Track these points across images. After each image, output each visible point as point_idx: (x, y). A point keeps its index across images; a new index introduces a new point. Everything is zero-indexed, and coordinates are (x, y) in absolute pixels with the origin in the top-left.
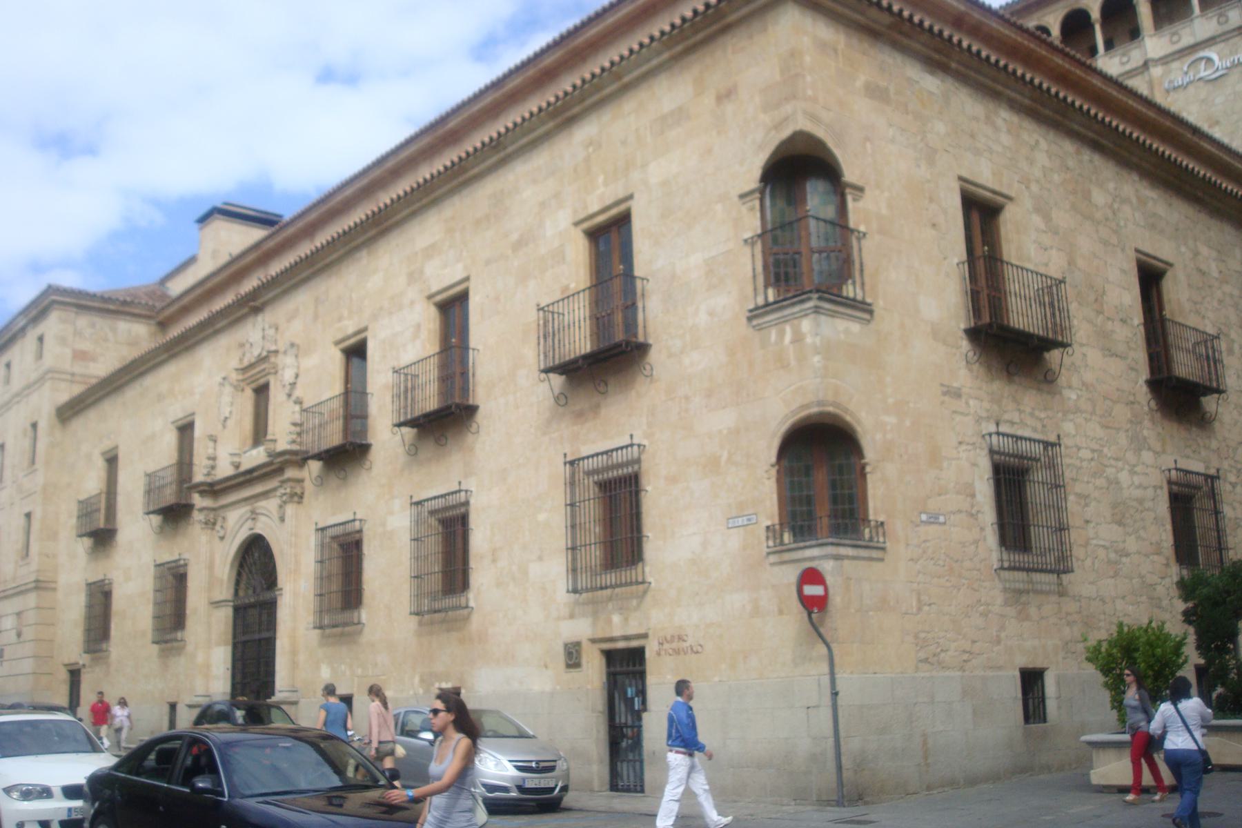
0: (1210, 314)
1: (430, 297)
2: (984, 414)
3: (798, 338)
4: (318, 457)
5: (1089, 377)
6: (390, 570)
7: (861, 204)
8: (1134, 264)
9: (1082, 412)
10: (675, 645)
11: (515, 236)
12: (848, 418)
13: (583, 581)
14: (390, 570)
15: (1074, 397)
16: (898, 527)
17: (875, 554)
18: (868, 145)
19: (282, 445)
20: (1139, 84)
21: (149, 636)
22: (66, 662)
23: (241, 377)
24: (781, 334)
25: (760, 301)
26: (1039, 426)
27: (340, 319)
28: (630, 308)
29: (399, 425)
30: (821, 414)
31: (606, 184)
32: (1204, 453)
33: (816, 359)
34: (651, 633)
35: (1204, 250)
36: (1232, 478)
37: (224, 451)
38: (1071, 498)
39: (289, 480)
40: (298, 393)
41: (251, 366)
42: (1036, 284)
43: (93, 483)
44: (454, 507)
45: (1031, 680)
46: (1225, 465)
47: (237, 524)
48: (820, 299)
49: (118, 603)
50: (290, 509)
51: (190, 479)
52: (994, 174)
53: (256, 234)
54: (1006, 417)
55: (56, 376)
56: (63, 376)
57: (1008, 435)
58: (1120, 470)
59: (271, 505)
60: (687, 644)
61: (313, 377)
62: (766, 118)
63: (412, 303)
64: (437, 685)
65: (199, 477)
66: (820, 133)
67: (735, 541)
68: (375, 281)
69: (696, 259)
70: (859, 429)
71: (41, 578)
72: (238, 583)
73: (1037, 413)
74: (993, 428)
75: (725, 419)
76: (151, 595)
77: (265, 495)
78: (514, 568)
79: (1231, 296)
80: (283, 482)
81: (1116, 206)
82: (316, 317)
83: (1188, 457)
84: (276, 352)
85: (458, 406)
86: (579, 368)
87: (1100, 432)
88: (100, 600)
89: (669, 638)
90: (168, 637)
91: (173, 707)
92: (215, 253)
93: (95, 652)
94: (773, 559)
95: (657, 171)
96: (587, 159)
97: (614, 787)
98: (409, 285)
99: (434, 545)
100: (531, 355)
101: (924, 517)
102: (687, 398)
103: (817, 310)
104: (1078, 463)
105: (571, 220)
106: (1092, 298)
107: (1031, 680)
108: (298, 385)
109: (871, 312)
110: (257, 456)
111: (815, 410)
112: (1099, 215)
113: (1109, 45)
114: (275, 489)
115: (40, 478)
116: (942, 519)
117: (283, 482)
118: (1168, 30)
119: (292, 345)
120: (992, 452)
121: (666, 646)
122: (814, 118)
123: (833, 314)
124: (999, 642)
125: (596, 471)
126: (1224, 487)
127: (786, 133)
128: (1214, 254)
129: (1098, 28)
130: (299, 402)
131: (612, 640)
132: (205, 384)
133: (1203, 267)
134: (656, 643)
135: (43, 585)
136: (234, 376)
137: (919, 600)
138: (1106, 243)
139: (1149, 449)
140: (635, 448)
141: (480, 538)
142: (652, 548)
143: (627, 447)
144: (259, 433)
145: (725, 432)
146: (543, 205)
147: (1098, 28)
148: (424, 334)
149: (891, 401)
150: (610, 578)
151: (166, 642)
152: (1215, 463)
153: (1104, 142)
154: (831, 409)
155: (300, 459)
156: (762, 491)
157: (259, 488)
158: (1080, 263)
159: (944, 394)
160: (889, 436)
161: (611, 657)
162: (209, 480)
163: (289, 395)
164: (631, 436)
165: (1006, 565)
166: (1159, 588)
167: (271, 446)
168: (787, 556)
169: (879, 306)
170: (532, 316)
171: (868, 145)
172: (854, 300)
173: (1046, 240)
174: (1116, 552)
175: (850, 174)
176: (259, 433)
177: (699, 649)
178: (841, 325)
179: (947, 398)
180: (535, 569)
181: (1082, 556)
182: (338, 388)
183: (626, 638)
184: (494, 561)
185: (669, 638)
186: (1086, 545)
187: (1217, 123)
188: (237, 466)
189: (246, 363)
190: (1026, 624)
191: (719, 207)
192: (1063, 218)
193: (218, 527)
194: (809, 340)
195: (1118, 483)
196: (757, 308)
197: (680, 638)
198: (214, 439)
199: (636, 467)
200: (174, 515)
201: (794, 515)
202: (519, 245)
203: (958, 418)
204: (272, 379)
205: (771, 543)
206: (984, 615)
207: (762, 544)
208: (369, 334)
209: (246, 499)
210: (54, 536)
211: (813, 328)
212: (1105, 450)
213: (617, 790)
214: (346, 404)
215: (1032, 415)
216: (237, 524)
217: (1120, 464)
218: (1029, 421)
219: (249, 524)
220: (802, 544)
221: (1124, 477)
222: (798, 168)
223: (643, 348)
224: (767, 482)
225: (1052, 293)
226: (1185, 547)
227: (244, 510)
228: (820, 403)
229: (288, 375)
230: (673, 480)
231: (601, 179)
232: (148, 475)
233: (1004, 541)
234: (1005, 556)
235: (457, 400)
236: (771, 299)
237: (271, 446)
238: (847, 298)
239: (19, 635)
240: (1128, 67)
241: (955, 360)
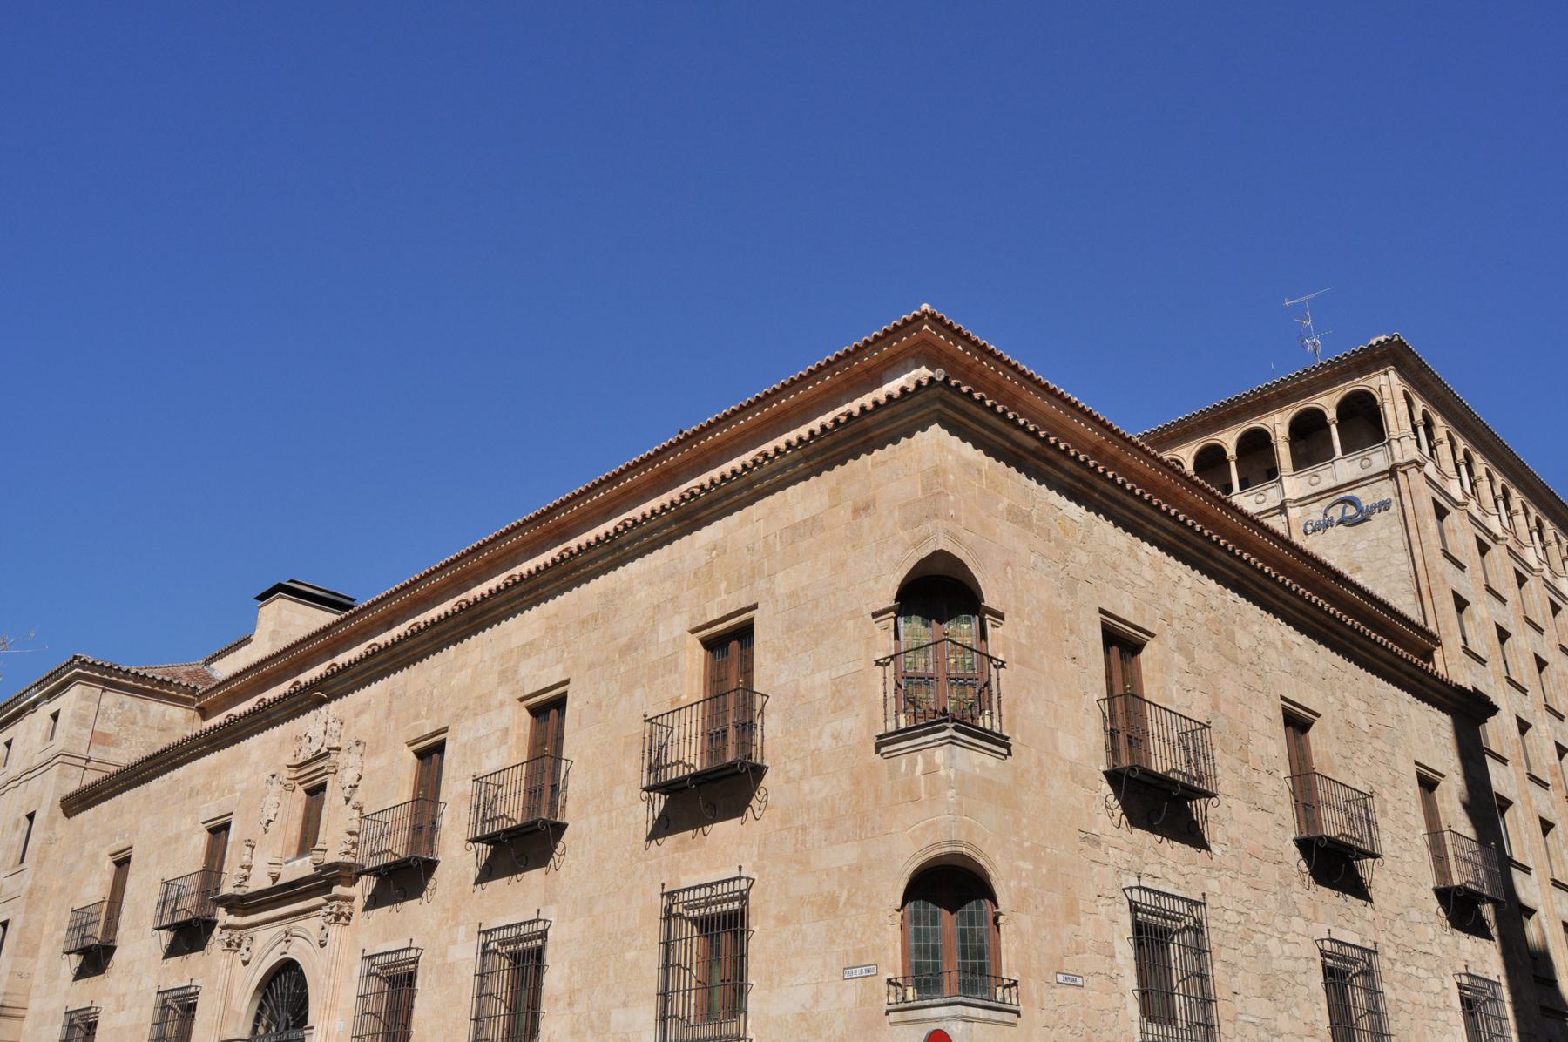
0: (1360, 771)
1: (522, 699)
2: (1124, 866)
3: (930, 770)
4: (375, 872)
5: (1233, 831)
7: (999, 631)
8: (1280, 712)
9: (1228, 869)
11: (624, 640)
12: (981, 861)
16: (1031, 987)
17: (1007, 1017)
18: (1009, 569)
19: (331, 857)
20: (1276, 523)
23: (293, 775)
24: (913, 764)
26: (1182, 881)
27: (417, 717)
28: (747, 727)
29: (474, 841)
30: (953, 855)
31: (728, 592)
32: (1358, 924)
33: (951, 793)
35: (1353, 703)
36: (1390, 953)
37: (262, 861)
38: (1217, 965)
39: (336, 898)
40: (357, 797)
41: (307, 763)
42: (1179, 726)
43: (95, 889)
46: (1382, 939)
47: (267, 944)
48: (956, 729)
50: (334, 931)
51: (218, 889)
53: (325, 618)
54: (1148, 870)
55: (68, 759)
56: (77, 761)
57: (1149, 890)
59: (312, 925)
61: (377, 781)
62: (904, 535)
63: (502, 704)
65: (227, 889)
66: (961, 554)
69: (823, 677)
70: (992, 874)
72: (258, 1018)
73: (1179, 867)
74: (1134, 882)
79: (1383, 752)
80: (330, 900)
81: (1260, 649)
83: (1342, 927)
84: (339, 749)
85: (544, 822)
87: (1247, 894)
92: (274, 634)
95: (784, 583)
96: (710, 564)
98: (500, 684)
99: (501, 983)
100: (634, 773)
101: (1060, 978)
103: (952, 740)
104: (1223, 926)
105: (688, 627)
106: (1236, 746)
109: (1008, 747)
110: (303, 867)
112: (1242, 658)
113: (1244, 485)
114: (319, 907)
115: (27, 880)
116: (1079, 981)
118: (1307, 473)
119: (358, 743)
120: (1134, 908)
122: (955, 538)
123: (969, 746)
126: (1382, 963)
127: (926, 551)
128: (1364, 706)
129: (1233, 464)
132: (250, 779)
136: (285, 774)
138: (1250, 688)
139: (1300, 915)
142: (753, 1000)
144: (308, 840)
146: (657, 608)
147: (1233, 464)
148: (512, 740)
149: (1027, 844)
154: (964, 850)
155: (343, 873)
156: (885, 939)
158: (1223, 707)
159: (1083, 840)
160: (1024, 884)
162: (239, 892)
163: (348, 800)
167: (319, 856)
168: (910, 1015)
170: (638, 727)
171: (1009, 569)
172: (991, 732)
173: (1189, 680)
174: (1267, 1030)
175: (990, 600)
176: (308, 840)
178: (977, 757)
179: (1085, 845)
180: (617, 1017)
181: (1230, 1034)
182: (407, 794)
186: (1235, 1021)
187: (1359, 569)
188: (275, 880)
189: (301, 759)
191: (850, 624)
192: (1206, 659)
193: (243, 950)
194: (942, 772)
196: (887, 735)
200: (188, 936)
201: (918, 968)
202: (626, 650)
203: (1097, 867)
204: (329, 779)
207: (883, 997)
210: (32, 951)
211: (950, 759)
212: (1253, 913)
214: (416, 815)
217: (1269, 930)
218: (1172, 876)
219: (282, 947)
220: (927, 1002)
221: (1273, 944)
222: (938, 591)
223: (759, 771)
224: (890, 928)
225: (1194, 736)
227: (277, 930)
228: (951, 843)
230: (784, 920)
231: (723, 586)
232: (166, 883)
233: (1147, 1013)
235: (544, 817)
237: (319, 856)
238: (984, 730)
240: (1264, 507)
241: (1100, 807)
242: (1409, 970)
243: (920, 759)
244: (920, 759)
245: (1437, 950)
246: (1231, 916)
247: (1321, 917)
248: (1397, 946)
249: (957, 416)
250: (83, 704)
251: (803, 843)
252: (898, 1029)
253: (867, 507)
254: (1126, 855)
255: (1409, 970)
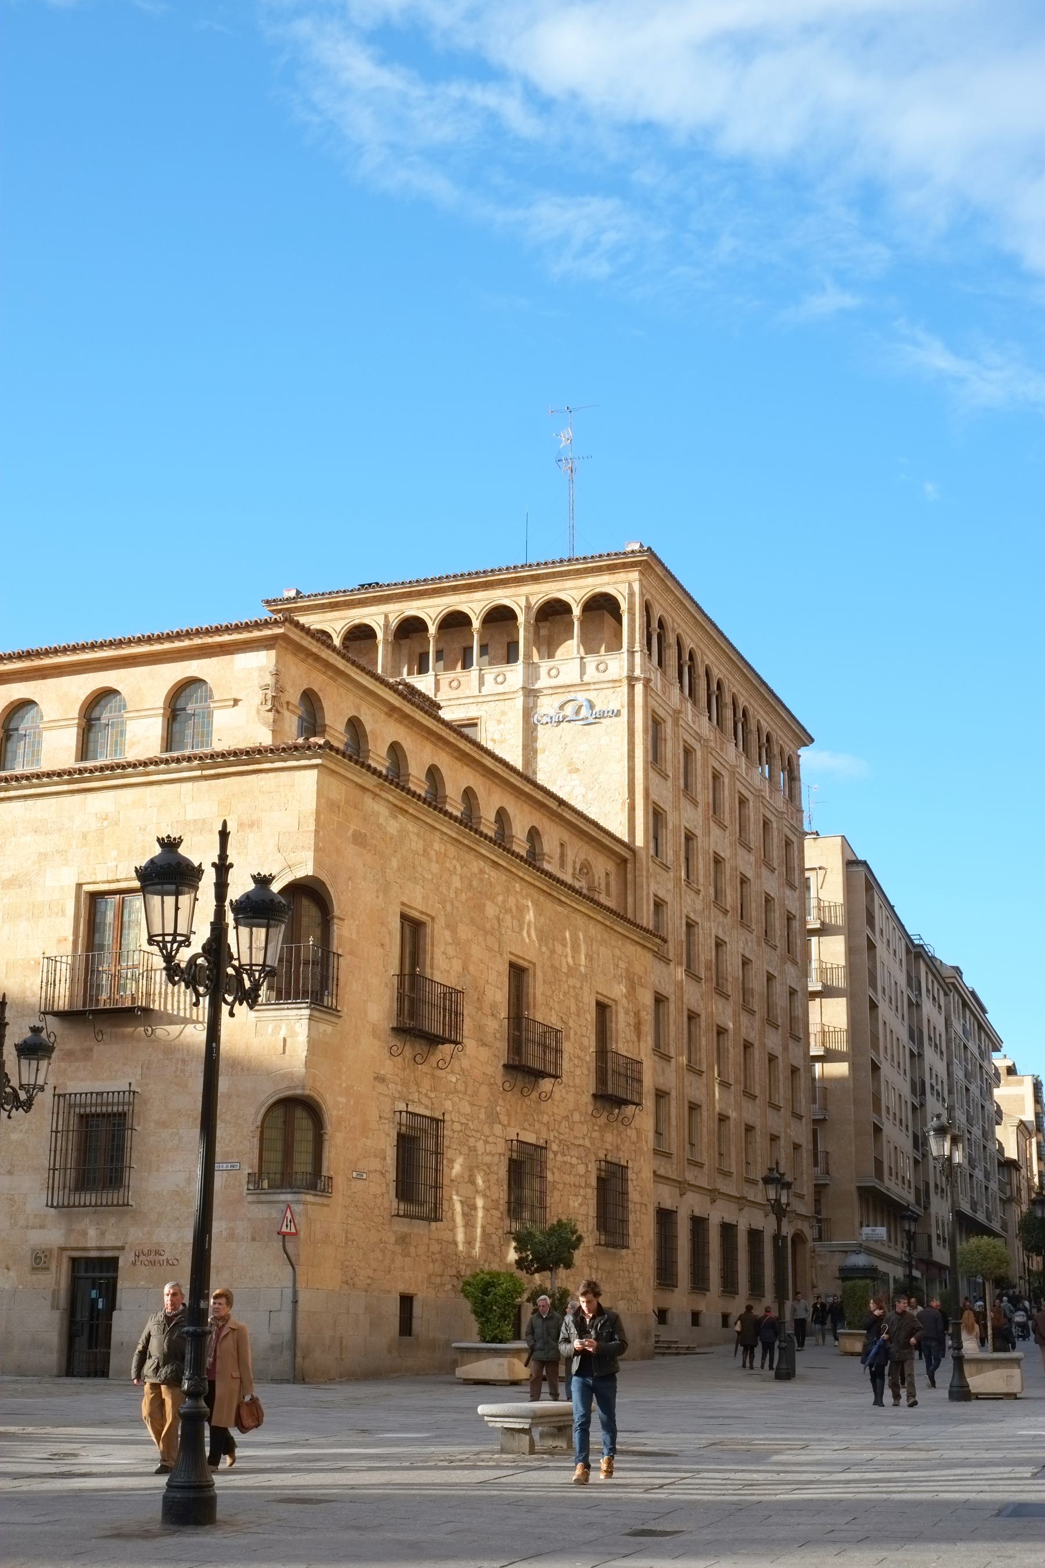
0: (556, 1006)
2: (397, 1095)
10: (151, 1258)
15: (454, 1080)
16: (339, 1182)
45: (406, 1301)
52: (423, 898)
58: (478, 1140)
60: (164, 1258)
74: (402, 1106)
79: (574, 987)
81: (501, 916)
87: (468, 1109)
89: (146, 1251)
101: (355, 1174)
107: (406, 1301)
111: (299, 1092)
112: (488, 926)
121: (142, 1258)
124: (389, 1272)
133: (557, 964)
137: (347, 1237)
138: (489, 949)
139: (500, 1123)
142: (133, 1179)
146: (43, 856)
149: (344, 1085)
152: (544, 1135)
153: (500, 862)
158: (472, 968)
160: (341, 1113)
165: (401, 1213)
166: (494, 1237)
168: (264, 1198)
169: (344, 1009)
173: (451, 951)
177: (176, 1262)
179: (377, 1083)
183: (100, 1249)
185: (146, 1251)
190: (407, 1259)
195: (475, 1150)
197: (157, 1253)
205: (251, 1187)
206: (382, 1251)
215: (426, 1095)
221: (480, 1145)
225: (452, 998)
226: (515, 1207)
234: (402, 1207)
242: (565, 1159)
243: (284, 1027)
244: (284, 1027)
245: (587, 1143)
246: (457, 1127)
247: (513, 1124)
248: (560, 1141)
249: (683, 1467)
251: (183, 1071)
252: (254, 1206)
253: (251, 825)
254: (399, 1088)
255: (565, 1159)
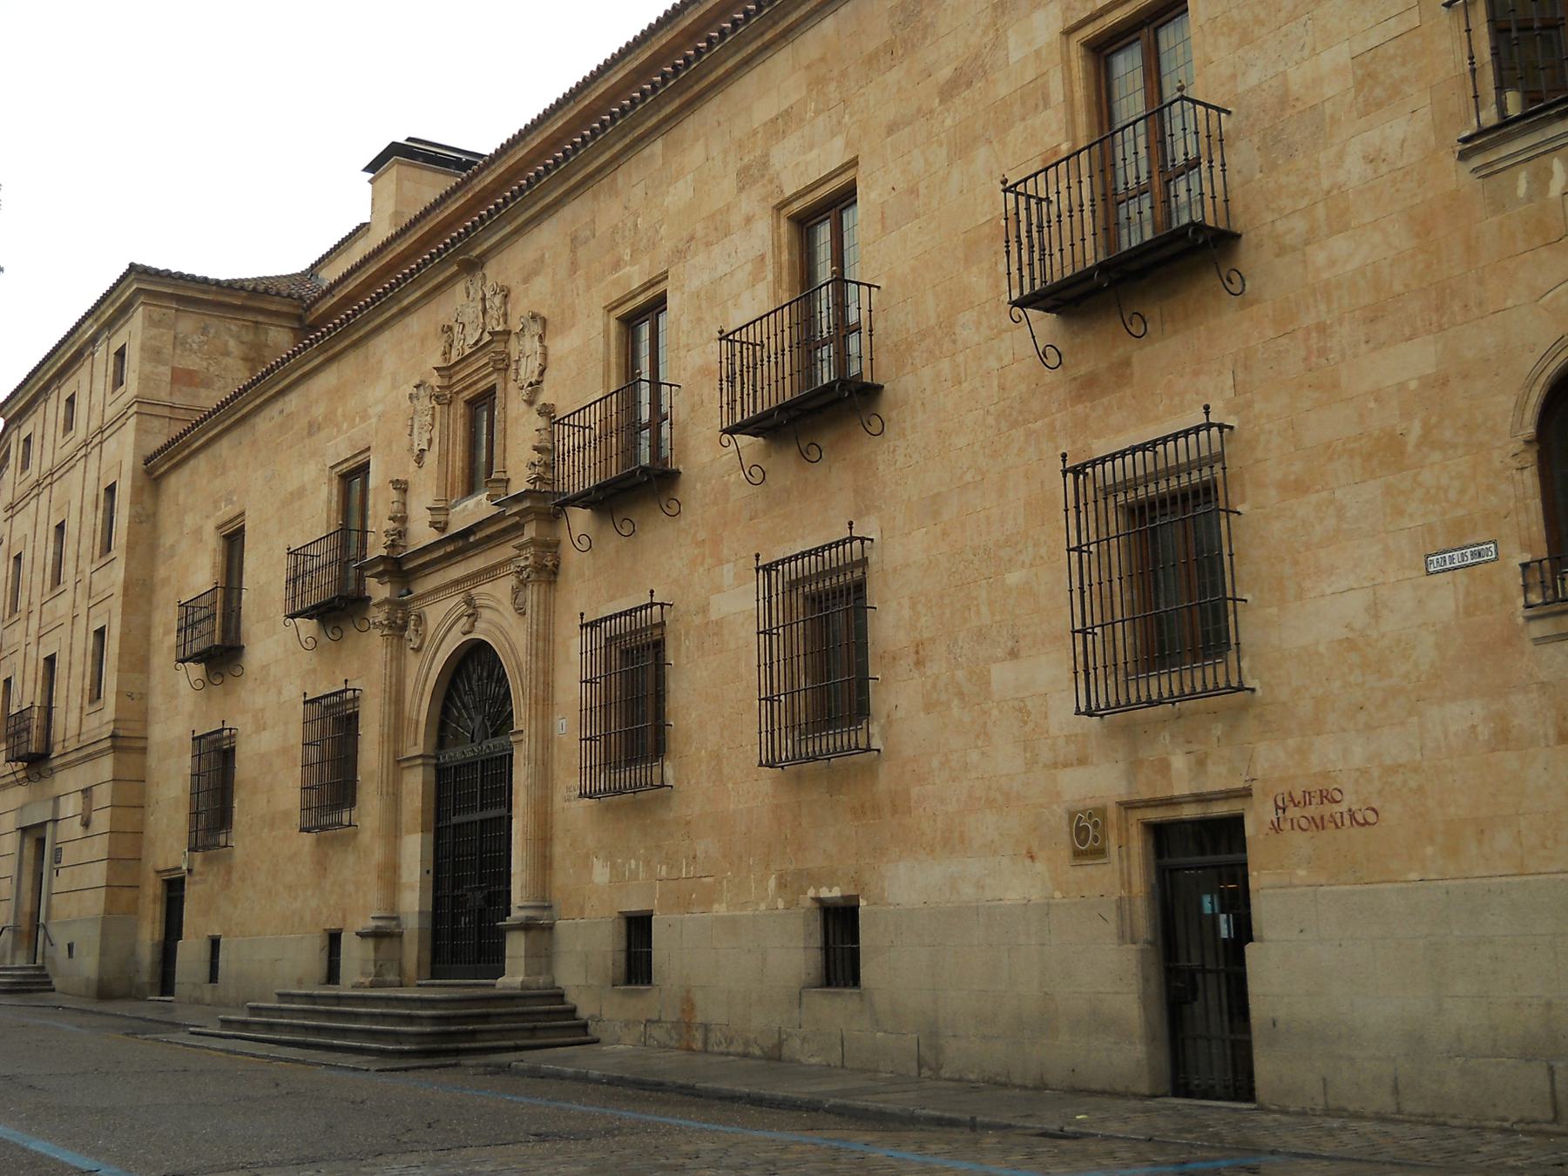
6: (721, 687)
10: (1313, 810)
11: (946, 72)
13: (785, 746)
14: (721, 687)
21: (296, 819)
22: (161, 867)
25: (1490, 116)
27: (617, 265)
29: (732, 431)
34: (1256, 786)
40: (544, 397)
44: (837, 571)
49: (245, 767)
56: (158, 411)
60: (1344, 807)
63: (749, 220)
64: (811, 893)
67: (1445, 599)
68: (678, 195)
69: (1341, 53)
71: (121, 733)
75: (1414, 360)
76: (298, 752)
77: (490, 573)
78: (960, 674)
82: (574, 267)
86: (1098, 290)
88: (217, 759)
89: (1298, 796)
90: (326, 820)
91: (334, 938)
93: (206, 848)
94: (1537, 629)
97: (1181, 1087)
98: (741, 189)
100: (990, 281)
102: (1322, 329)
105: (1058, 26)
108: (545, 385)
110: (477, 508)
114: (510, 561)
115: (63, 604)
117: (520, 547)
121: (1293, 812)
125: (1128, 485)
130: (547, 411)
131: (1170, 802)
132: (380, 399)
134: (1270, 806)
135: (126, 743)
140: (857, 543)
141: (891, 622)
143: (844, 542)
144: (477, 472)
145: (1413, 385)
150: (1160, 684)
151: (323, 828)
157: (477, 563)
161: (1161, 836)
164: (1207, 408)
176: (477, 472)
177: (1371, 817)
180: (1003, 675)
183: (1200, 799)
184: (919, 663)
196: (1482, 132)
197: (1325, 797)
198: (402, 487)
199: (858, 573)
202: (948, 91)
205: (1535, 598)
208: (668, 285)
209: (457, 582)
213: (1189, 1094)
214: (344, 546)
216: (443, 624)
227: (452, 603)
229: (528, 370)
230: (1299, 487)
236: (1513, 110)
239: (86, 824)
250: (153, 332)
